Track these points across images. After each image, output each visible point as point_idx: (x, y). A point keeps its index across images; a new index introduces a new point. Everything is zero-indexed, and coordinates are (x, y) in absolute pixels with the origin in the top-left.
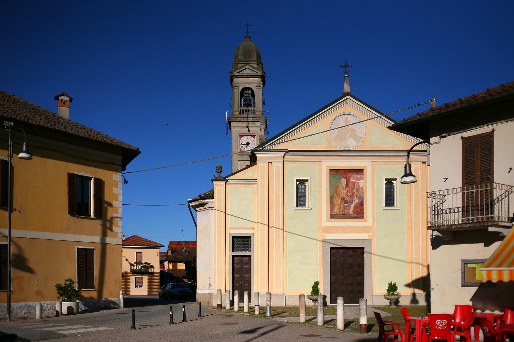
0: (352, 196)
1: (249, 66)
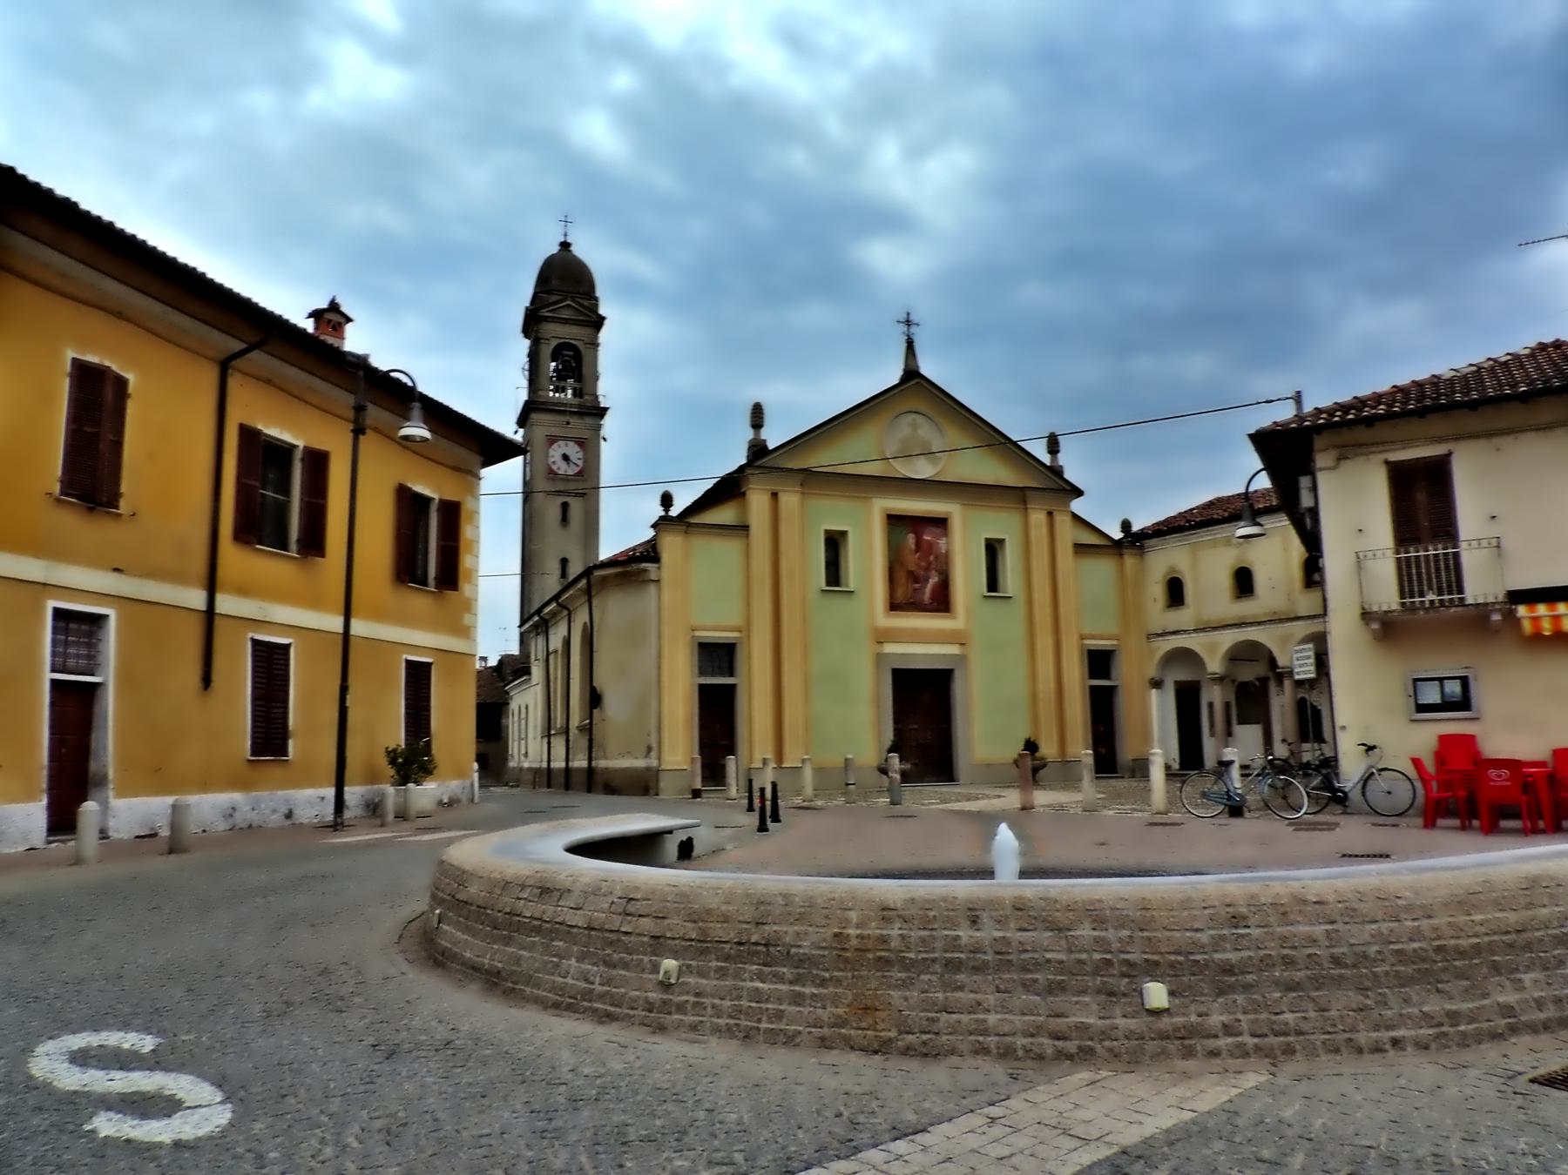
0: (927, 569)
1: (574, 301)
